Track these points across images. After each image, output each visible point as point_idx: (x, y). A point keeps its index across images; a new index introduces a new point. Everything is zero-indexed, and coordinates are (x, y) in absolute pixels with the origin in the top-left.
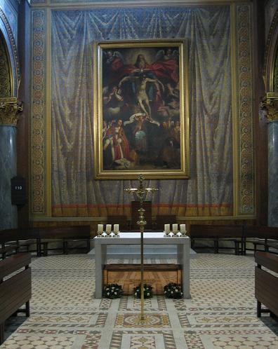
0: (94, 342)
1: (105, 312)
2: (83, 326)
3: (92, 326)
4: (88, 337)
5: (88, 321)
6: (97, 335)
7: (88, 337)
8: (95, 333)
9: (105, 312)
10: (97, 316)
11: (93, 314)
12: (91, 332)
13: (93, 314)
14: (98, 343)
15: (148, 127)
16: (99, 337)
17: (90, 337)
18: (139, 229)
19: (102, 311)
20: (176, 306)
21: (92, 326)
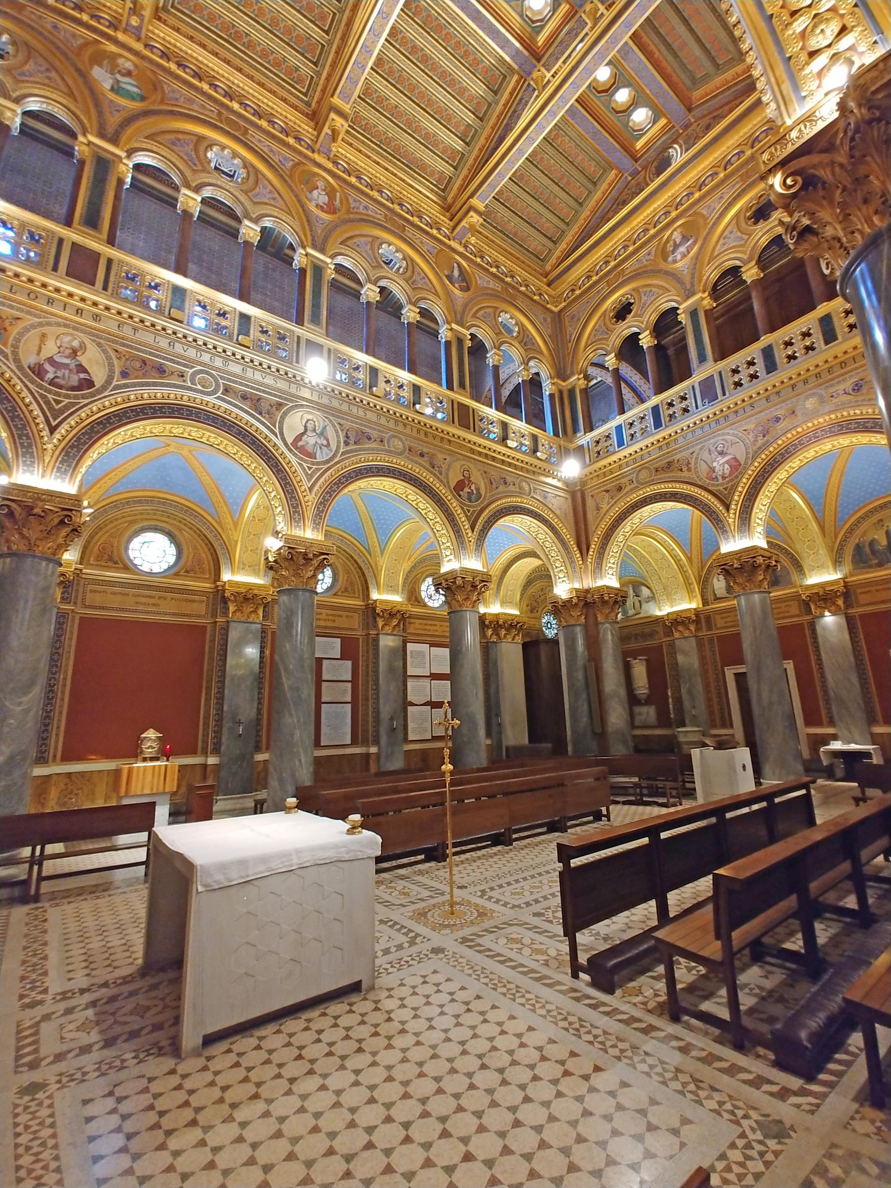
0: (38, 984)
1: (28, 1077)
2: (69, 1011)
3: (46, 1017)
4: (45, 991)
5: (62, 1027)
6: (27, 1000)
7: (45, 991)
8: (33, 1005)
9: (28, 1077)
10: (43, 1052)
11: (59, 1057)
12: (41, 1002)
13: (59, 1057)
14: (46, 985)
15: (134, 752)
16: (22, 997)
17: (40, 993)
18: (798, 628)
19: (36, 1076)
20: (674, 1009)
21: (46, 1017)
